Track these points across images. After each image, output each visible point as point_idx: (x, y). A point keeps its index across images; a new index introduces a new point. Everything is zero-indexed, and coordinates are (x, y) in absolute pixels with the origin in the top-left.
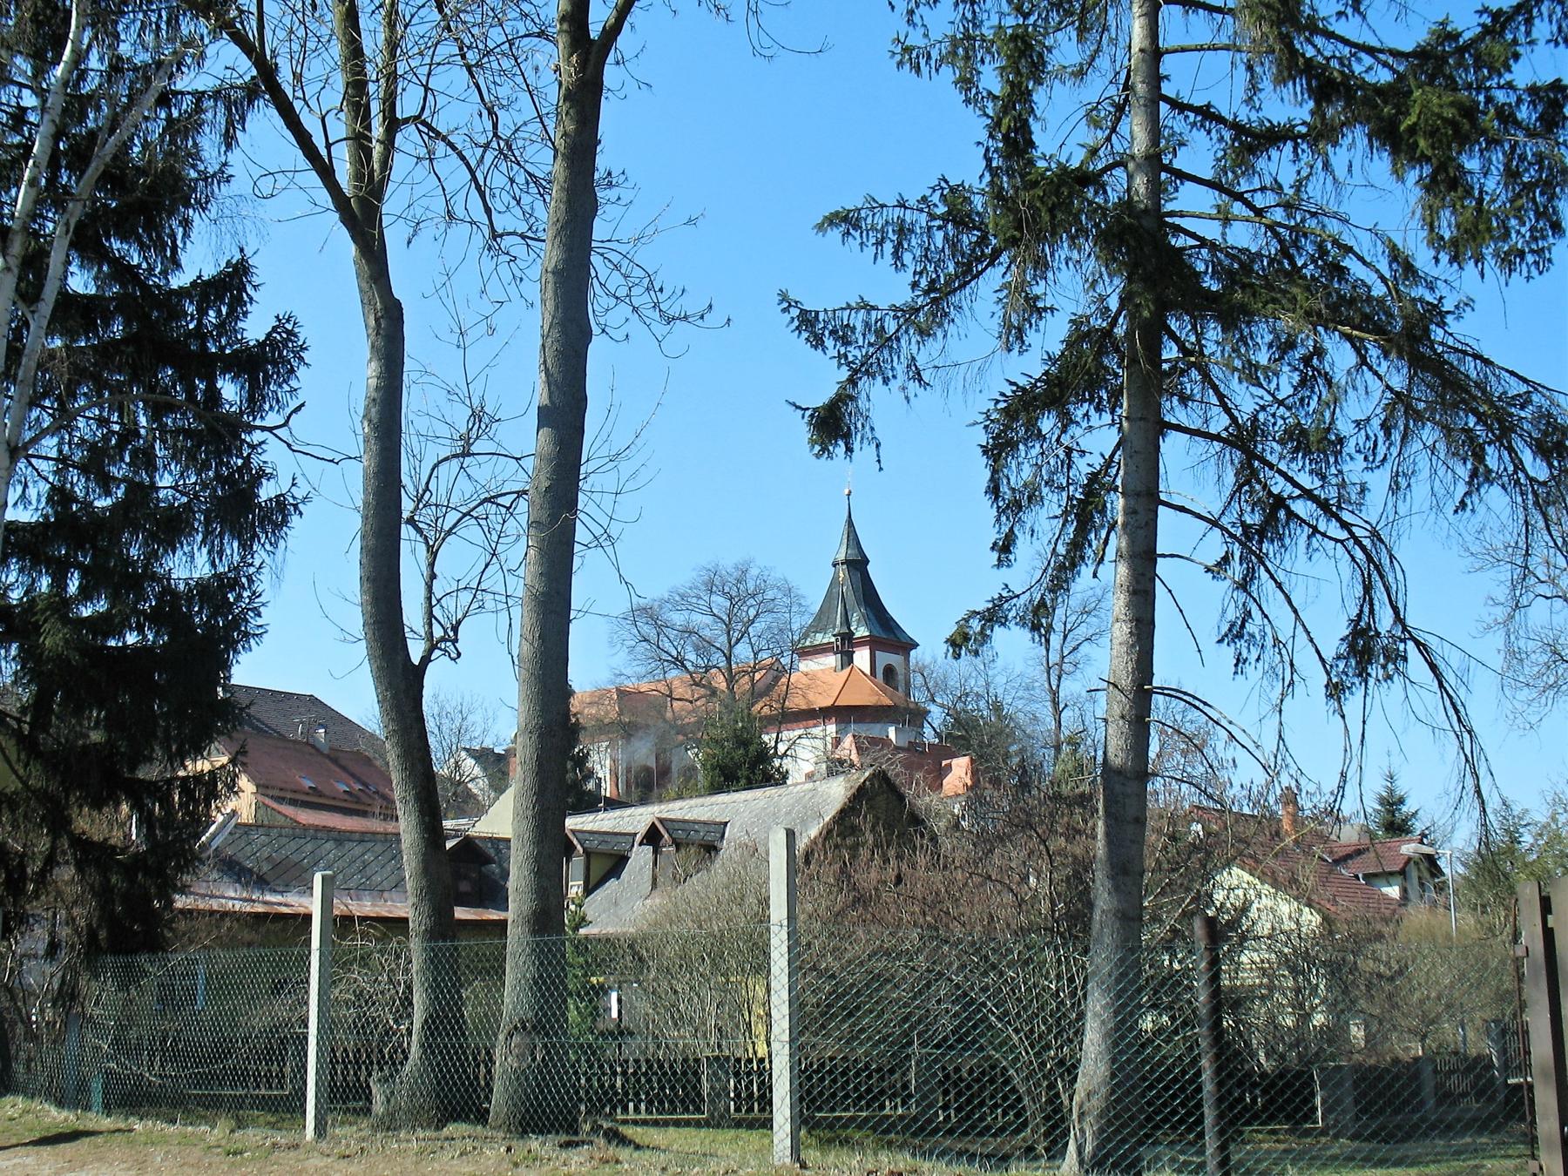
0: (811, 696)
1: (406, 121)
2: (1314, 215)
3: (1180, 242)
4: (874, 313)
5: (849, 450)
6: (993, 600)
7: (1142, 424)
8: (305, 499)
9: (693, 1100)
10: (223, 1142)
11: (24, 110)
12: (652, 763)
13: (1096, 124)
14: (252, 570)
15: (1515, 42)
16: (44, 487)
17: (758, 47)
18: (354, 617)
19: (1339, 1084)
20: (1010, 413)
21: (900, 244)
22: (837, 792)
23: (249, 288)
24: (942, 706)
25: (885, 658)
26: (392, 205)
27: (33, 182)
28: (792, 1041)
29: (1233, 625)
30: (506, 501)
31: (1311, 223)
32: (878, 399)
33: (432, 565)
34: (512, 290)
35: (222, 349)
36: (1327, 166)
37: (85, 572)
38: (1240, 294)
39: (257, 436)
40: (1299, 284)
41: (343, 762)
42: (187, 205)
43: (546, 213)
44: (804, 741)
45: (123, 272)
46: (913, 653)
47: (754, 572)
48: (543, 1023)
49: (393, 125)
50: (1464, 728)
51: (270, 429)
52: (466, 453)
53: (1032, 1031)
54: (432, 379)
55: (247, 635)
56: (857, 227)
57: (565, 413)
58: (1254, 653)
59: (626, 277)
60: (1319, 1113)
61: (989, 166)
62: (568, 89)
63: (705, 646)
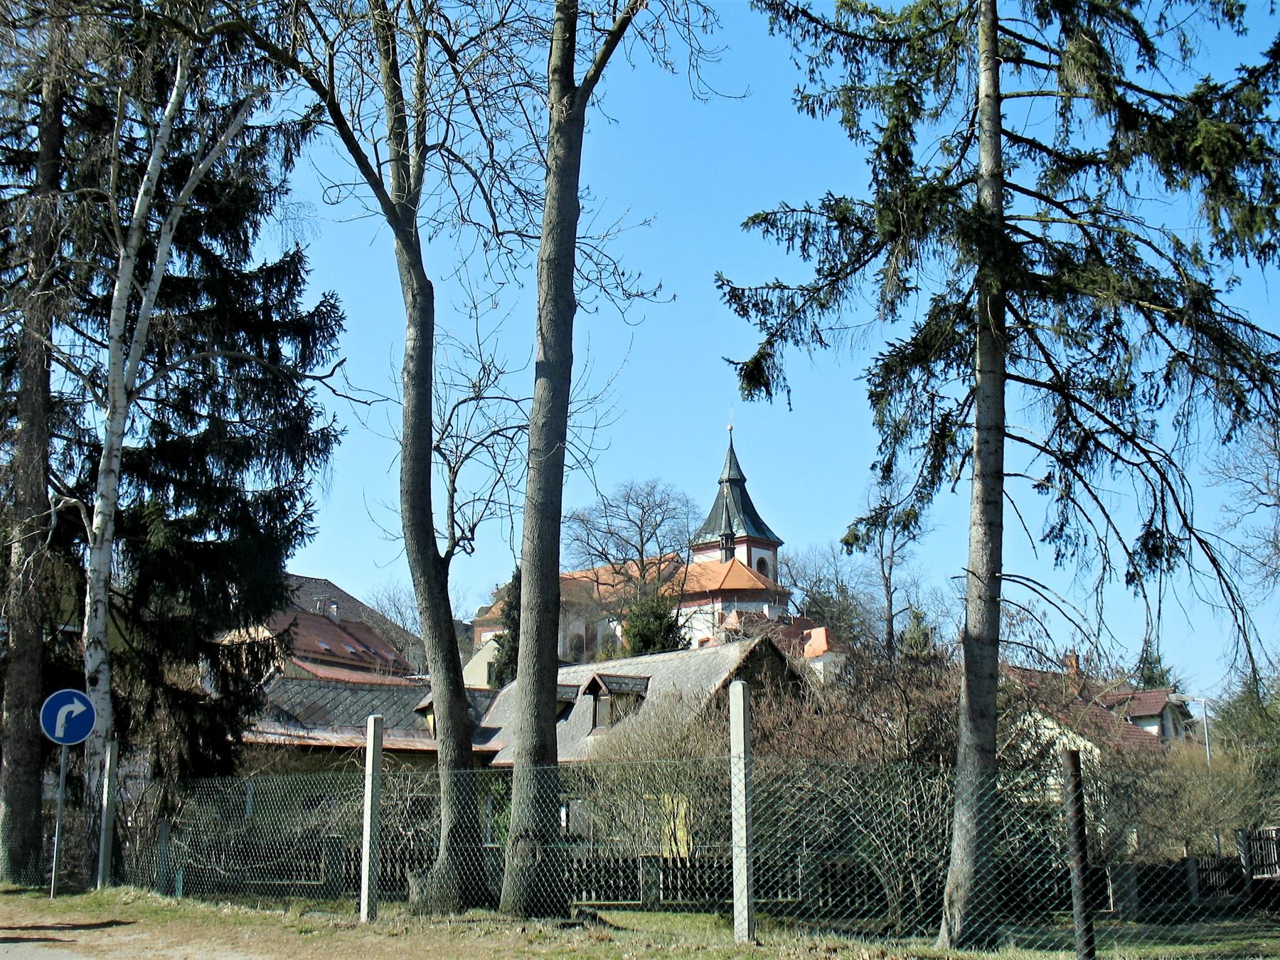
0: (703, 582)
1: (433, 147)
2: (1116, 219)
3: (1021, 238)
4: (786, 291)
5: (769, 393)
6: (875, 510)
7: (991, 375)
8: (343, 431)
9: (631, 890)
10: (296, 923)
11: (135, 140)
12: (582, 632)
13: (950, 153)
14: (303, 485)
15: (1266, 92)
16: (147, 422)
17: (697, 93)
18: (395, 521)
19: (1126, 880)
20: (888, 369)
21: (806, 239)
22: (734, 654)
23: (302, 273)
24: (802, 589)
25: (758, 553)
26: (424, 211)
27: (146, 193)
28: (748, 847)
29: (1053, 528)
30: (510, 433)
31: (1113, 225)
32: (789, 357)
33: (453, 482)
34: (509, 273)
35: (283, 318)
36: (1121, 184)
37: (179, 486)
38: (1067, 279)
39: (308, 384)
40: (1097, 272)
41: (350, 630)
42: (256, 211)
43: (541, 217)
44: (698, 616)
45: (210, 260)
46: (779, 549)
47: (660, 488)
48: (544, 831)
49: (424, 150)
50: (1237, 606)
51: (320, 379)
52: (478, 397)
53: (891, 836)
54: (452, 341)
55: (302, 534)
56: (773, 225)
57: (556, 369)
58: (1070, 549)
59: (597, 264)
60: (1111, 901)
61: (876, 179)
62: (559, 123)
63: (623, 544)
